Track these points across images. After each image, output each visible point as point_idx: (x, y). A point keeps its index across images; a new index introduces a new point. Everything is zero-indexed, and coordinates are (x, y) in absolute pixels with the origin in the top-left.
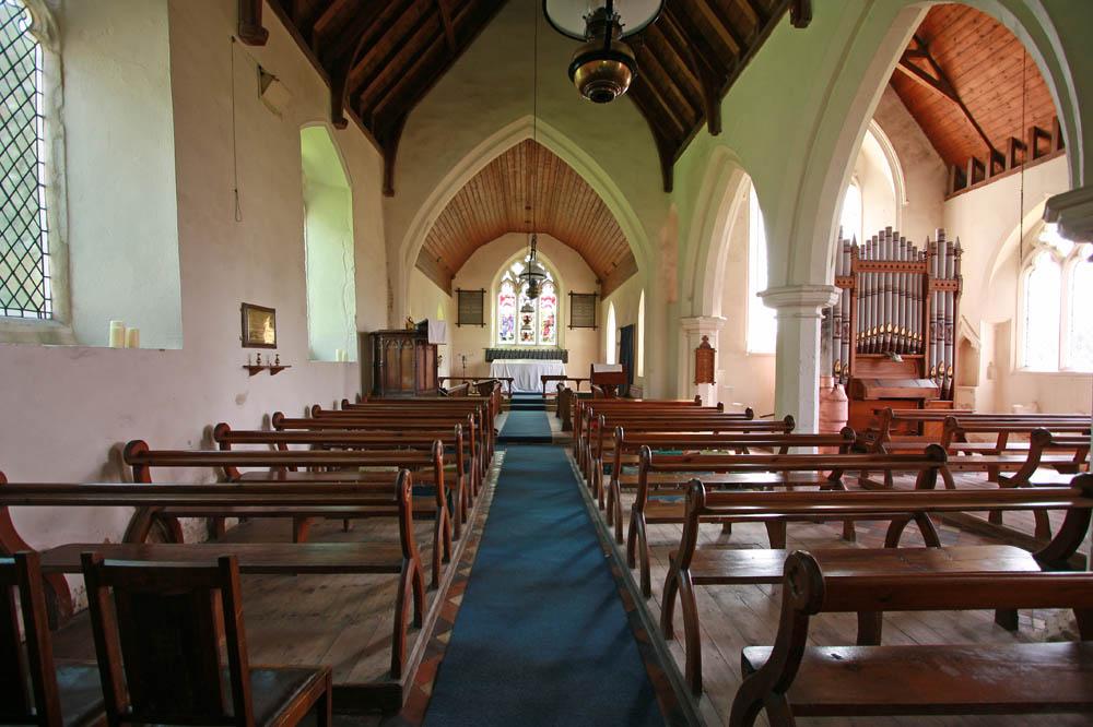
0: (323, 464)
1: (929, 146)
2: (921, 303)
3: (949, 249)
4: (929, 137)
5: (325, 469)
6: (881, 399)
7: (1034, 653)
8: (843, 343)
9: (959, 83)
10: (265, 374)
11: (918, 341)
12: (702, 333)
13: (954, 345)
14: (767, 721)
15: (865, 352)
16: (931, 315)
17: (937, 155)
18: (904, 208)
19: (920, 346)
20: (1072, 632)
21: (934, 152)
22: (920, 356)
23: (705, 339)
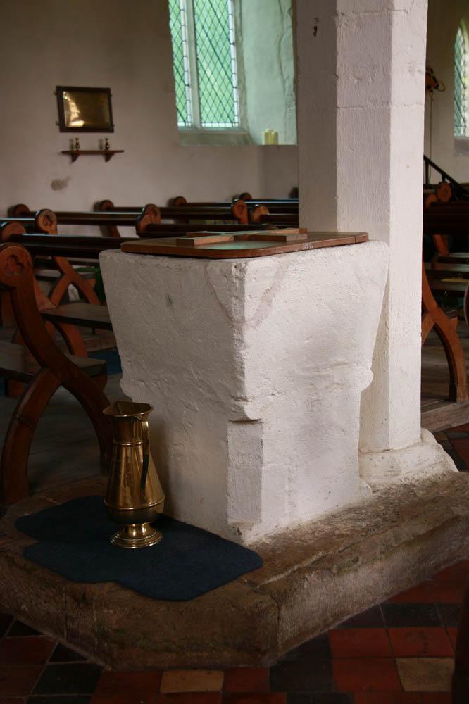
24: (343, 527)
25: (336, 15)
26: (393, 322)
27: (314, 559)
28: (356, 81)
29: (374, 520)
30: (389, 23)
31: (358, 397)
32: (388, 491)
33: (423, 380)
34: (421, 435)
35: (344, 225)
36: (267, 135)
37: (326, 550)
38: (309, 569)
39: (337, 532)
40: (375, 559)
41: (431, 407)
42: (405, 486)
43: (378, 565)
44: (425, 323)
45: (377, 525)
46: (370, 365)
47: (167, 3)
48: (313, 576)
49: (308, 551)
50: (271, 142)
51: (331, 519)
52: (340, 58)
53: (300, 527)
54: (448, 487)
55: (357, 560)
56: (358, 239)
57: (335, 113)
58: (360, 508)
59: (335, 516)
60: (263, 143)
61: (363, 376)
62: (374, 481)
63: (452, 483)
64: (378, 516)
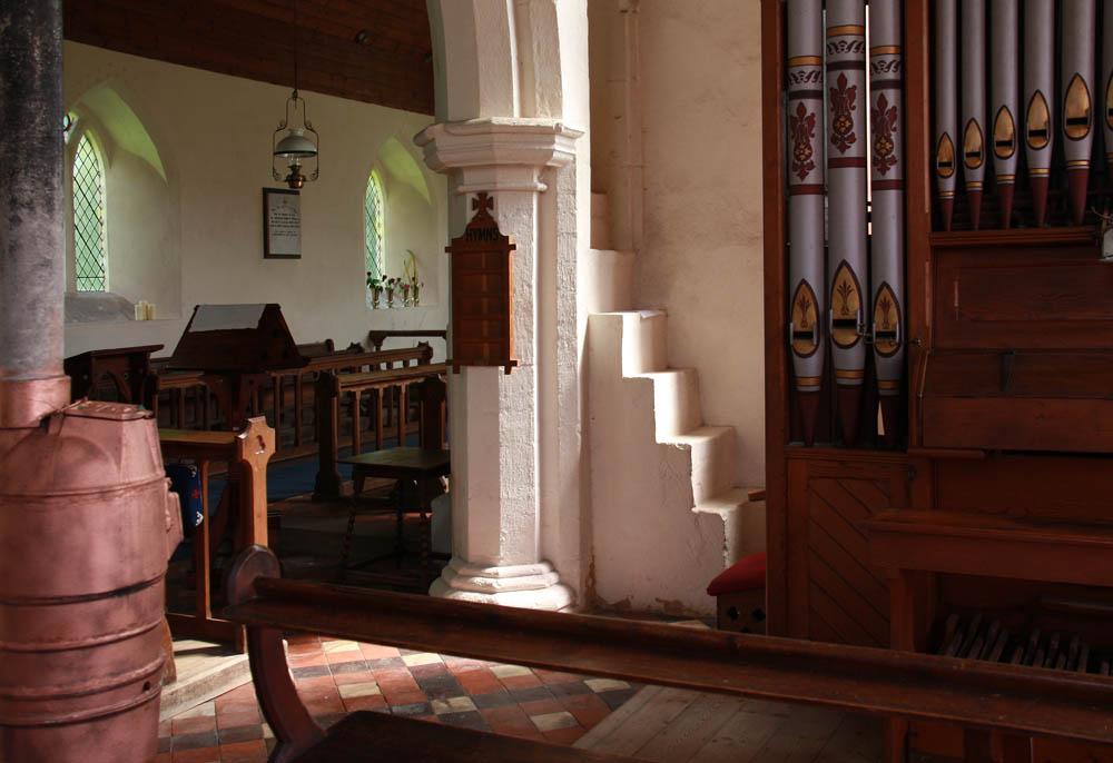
23: (484, 202)
53: (581, 575)
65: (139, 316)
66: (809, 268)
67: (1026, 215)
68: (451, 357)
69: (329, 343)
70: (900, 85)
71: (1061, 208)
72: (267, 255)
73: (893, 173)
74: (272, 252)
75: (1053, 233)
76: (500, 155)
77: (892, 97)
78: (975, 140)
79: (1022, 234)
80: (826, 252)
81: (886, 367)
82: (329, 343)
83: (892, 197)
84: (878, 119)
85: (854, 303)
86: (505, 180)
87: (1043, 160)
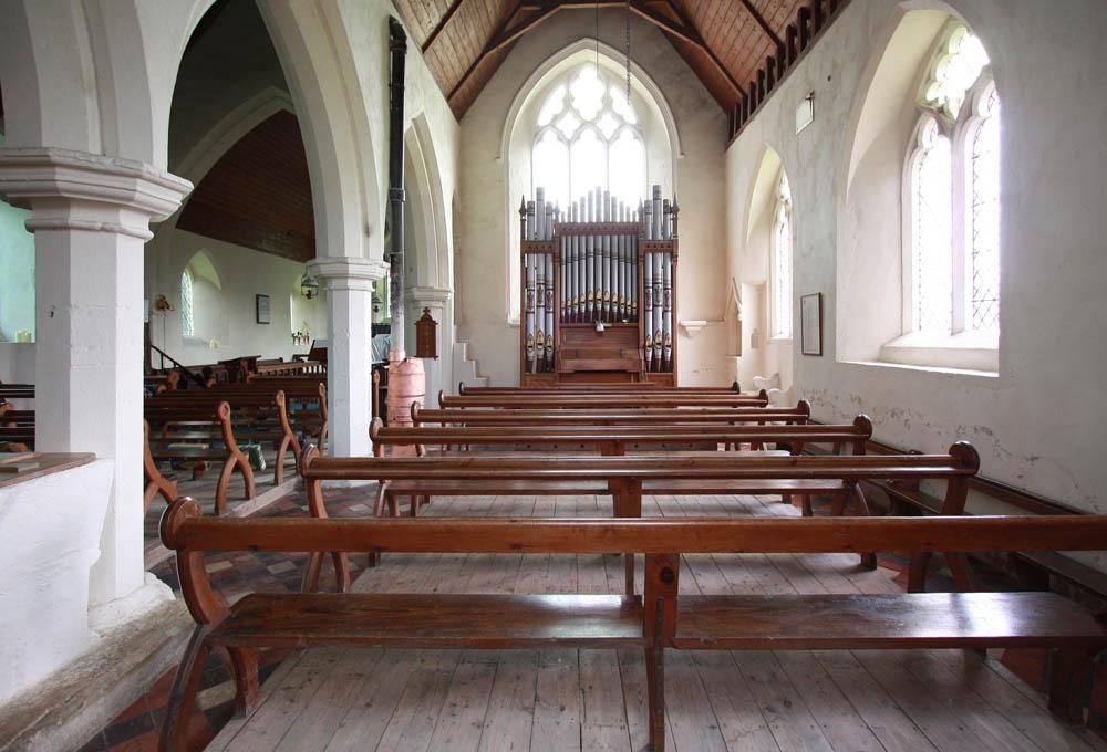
0: (455, 441)
1: (706, 94)
2: (635, 267)
3: (665, 207)
4: (704, 84)
5: (445, 446)
6: (576, 372)
7: (632, 631)
8: (546, 313)
9: (698, 20)
10: (922, 306)
11: (632, 308)
12: (424, 304)
13: (554, 312)
14: (666, 721)
15: (573, 321)
16: (645, 279)
17: (715, 103)
18: (679, 162)
19: (635, 313)
20: (893, 617)
21: (711, 100)
22: (633, 324)
23: (427, 310)
24: (71, 679)
25: (70, 306)
26: (119, 508)
27: (40, 718)
28: (86, 349)
29: (100, 663)
30: (114, 313)
31: (87, 572)
32: (114, 633)
33: (145, 407)
34: (147, 327)
35: (76, 447)
36: (20, 335)
37: (53, 705)
38: (34, 731)
39: (65, 685)
40: (98, 697)
41: (151, 548)
42: (129, 624)
43: (102, 700)
44: (148, 496)
45: (102, 667)
46: (98, 545)
47: (133, 3)
48: (38, 735)
49: (34, 712)
50: (23, 340)
51: (59, 675)
52: (73, 334)
53: (28, 692)
54: (165, 614)
55: (82, 704)
56: (87, 458)
57: (69, 370)
58: (87, 656)
59: (64, 670)
60: (16, 341)
61: (93, 554)
62: (101, 627)
63: (168, 610)
64: (105, 658)
65: (212, 345)
66: (532, 331)
67: (580, 321)
68: (262, 370)
69: (281, 359)
70: (545, 284)
71: (587, 320)
72: (258, 322)
73: (543, 304)
74: (261, 320)
75: (584, 324)
76: (64, 179)
77: (542, 287)
78: (569, 303)
79: (579, 325)
80: (536, 327)
81: (550, 354)
82: (281, 359)
83: (542, 310)
84: (821, 604)
85: (542, 339)
86: (434, 304)
87: (584, 309)
